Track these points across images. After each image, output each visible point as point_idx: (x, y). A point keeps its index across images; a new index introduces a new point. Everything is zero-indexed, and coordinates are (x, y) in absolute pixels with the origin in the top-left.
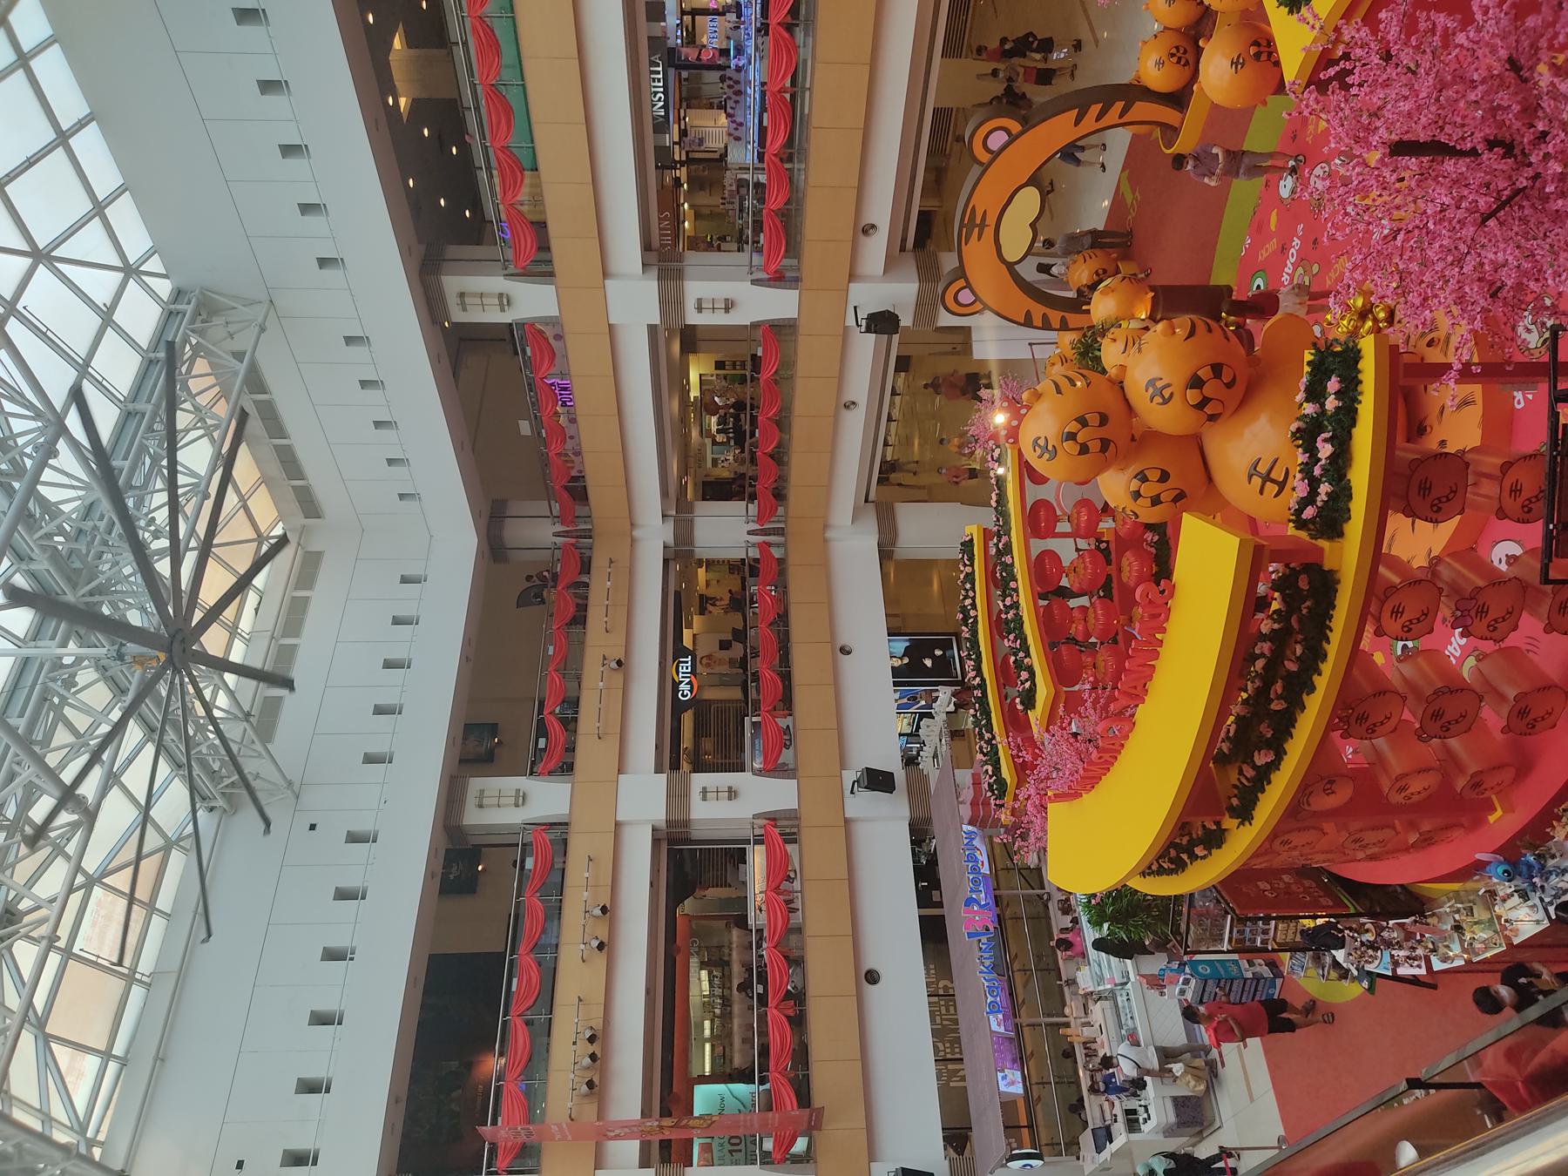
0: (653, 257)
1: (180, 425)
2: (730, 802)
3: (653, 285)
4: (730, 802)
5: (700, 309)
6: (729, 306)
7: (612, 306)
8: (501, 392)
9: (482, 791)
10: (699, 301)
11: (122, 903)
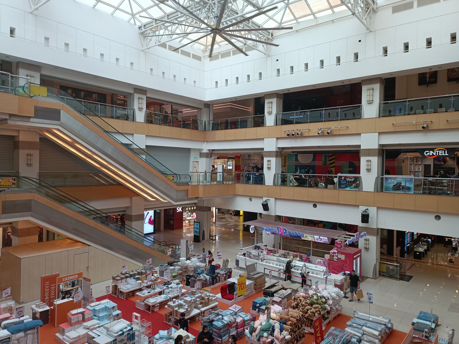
0: (211, 152)
1: (242, 32)
2: (369, 172)
3: (274, 149)
4: (369, 172)
5: (268, 161)
6: (269, 168)
7: (269, 140)
8: (244, 112)
10: (270, 161)
11: (116, 5)
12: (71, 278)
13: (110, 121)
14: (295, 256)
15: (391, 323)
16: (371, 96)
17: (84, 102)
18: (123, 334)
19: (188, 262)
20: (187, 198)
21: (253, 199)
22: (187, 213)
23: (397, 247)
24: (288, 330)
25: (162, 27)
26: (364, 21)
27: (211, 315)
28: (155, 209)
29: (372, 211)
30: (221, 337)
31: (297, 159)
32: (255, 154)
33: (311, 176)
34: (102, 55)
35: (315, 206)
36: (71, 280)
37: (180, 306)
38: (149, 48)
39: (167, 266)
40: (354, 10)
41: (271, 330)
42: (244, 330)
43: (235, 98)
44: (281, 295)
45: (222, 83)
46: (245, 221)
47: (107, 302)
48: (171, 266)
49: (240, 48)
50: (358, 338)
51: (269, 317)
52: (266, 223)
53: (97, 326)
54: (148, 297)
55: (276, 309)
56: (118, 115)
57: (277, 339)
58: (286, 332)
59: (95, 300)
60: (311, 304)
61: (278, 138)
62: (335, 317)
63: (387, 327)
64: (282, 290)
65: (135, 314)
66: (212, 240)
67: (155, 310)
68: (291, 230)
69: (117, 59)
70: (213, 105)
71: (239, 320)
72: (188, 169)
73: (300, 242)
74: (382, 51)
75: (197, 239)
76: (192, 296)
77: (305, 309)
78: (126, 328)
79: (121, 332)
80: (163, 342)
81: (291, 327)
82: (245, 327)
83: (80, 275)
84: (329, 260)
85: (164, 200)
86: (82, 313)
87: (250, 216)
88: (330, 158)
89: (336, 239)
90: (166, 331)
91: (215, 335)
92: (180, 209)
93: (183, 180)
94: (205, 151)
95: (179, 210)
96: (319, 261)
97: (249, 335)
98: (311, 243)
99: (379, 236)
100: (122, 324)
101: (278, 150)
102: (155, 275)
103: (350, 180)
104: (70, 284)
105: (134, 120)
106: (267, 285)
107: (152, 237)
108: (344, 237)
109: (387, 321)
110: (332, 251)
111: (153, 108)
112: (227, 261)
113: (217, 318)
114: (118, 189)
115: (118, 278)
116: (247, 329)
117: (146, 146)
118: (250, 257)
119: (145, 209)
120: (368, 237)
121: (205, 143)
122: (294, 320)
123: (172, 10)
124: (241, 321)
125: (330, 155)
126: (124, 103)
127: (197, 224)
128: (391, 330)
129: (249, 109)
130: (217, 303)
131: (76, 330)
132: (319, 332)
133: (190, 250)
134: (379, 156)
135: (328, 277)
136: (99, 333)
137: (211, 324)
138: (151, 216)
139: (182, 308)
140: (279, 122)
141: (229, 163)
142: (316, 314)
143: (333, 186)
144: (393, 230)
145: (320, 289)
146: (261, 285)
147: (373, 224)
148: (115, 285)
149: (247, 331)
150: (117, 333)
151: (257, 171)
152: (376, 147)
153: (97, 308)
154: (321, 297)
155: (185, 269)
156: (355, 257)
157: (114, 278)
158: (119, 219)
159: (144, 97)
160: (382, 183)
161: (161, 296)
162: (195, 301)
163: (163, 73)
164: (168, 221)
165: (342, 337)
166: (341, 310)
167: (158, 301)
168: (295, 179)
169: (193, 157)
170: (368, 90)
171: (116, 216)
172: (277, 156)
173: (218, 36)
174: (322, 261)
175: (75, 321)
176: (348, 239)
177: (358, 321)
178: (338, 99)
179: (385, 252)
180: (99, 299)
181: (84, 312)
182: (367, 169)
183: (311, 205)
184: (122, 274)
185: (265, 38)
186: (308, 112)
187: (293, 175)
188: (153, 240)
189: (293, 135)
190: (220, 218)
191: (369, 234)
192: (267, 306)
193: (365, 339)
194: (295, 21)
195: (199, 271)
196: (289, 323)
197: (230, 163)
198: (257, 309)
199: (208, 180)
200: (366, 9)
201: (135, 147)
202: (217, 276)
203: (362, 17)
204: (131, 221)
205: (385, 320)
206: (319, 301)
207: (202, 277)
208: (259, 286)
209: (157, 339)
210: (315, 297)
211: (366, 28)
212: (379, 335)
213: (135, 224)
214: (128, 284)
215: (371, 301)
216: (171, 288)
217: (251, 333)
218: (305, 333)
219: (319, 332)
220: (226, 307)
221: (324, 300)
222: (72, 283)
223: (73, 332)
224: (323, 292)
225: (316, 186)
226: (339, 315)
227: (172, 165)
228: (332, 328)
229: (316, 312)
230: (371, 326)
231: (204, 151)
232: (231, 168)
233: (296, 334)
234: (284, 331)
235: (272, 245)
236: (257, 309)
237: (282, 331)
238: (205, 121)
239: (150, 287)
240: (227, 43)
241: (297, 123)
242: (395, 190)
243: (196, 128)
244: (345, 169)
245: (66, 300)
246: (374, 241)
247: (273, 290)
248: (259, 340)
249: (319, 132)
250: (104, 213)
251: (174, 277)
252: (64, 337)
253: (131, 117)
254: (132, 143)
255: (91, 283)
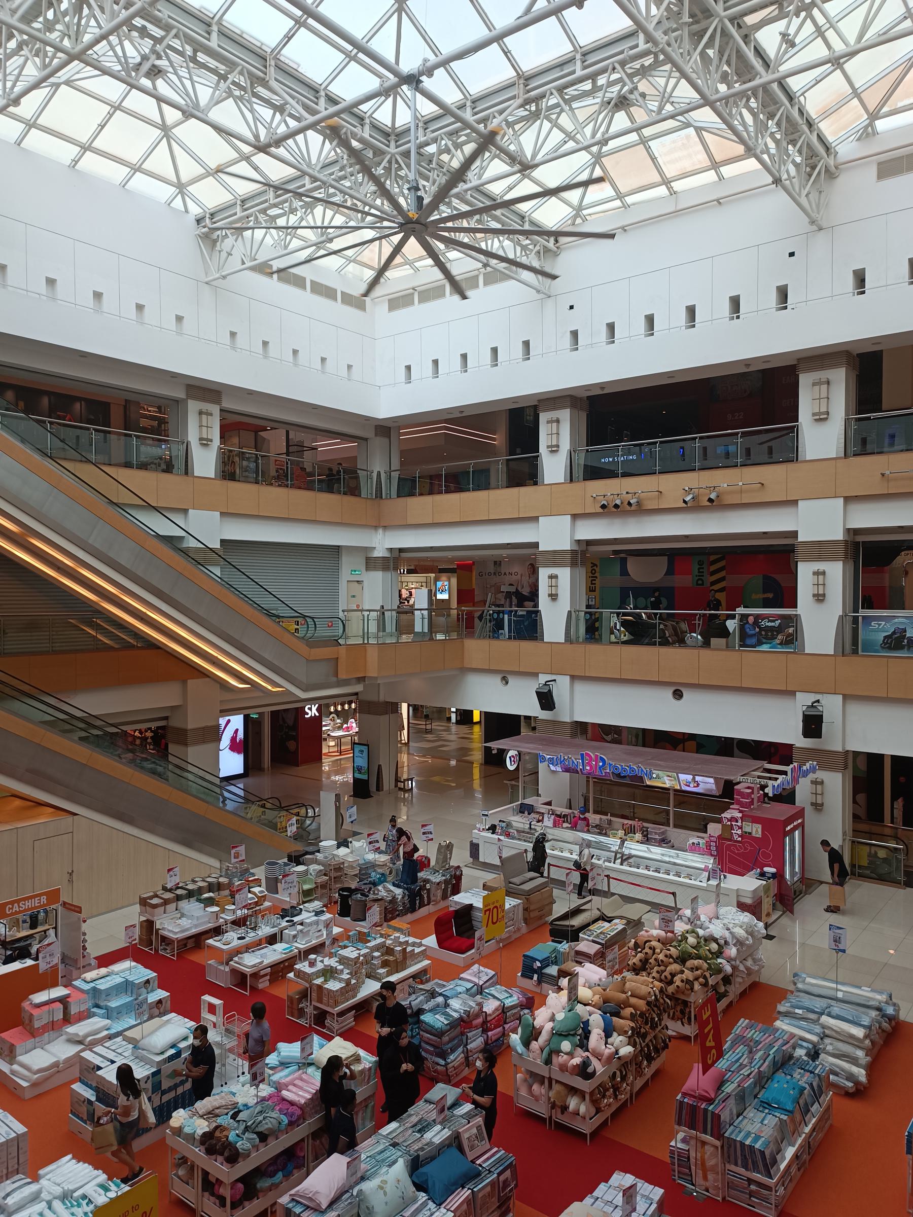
0: (396, 554)
2: (821, 604)
3: (566, 546)
4: (821, 604)
5: (551, 577)
6: (554, 597)
7: (551, 521)
8: (486, 446)
9: (211, 415)
10: (556, 577)
12: (28, 904)
13: (123, 474)
14: (630, 831)
15: (894, 1005)
16: (555, 436)
17: (51, 423)
18: (178, 1055)
19: (343, 851)
20: (335, 679)
21: (511, 680)
22: (333, 720)
23: (894, 799)
24: (626, 1032)
25: (262, 218)
26: (804, 201)
27: (414, 996)
28: (247, 712)
29: (831, 707)
30: (443, 1055)
31: (624, 572)
32: (513, 559)
33: (665, 617)
34: (98, 296)
35: (678, 695)
36: (29, 909)
37: (329, 973)
38: (224, 277)
39: (285, 864)
40: (779, 171)
41: (580, 1033)
42: (504, 1035)
43: (461, 409)
44: (597, 936)
45: (422, 370)
46: (488, 737)
47: (130, 969)
48: (299, 863)
49: (457, 278)
50: (810, 1046)
51: (573, 998)
52: (549, 743)
53: (105, 1033)
54: (238, 951)
55: (590, 974)
56: (143, 459)
57: (598, 1056)
58: (621, 1038)
59: (94, 963)
60: (682, 959)
61: (575, 517)
62: (744, 992)
63: (884, 1016)
64: (600, 923)
65: (207, 998)
66: (404, 790)
67: (261, 986)
68: (617, 760)
69: (140, 308)
70: (400, 428)
71: (490, 1006)
72: (336, 601)
73: (637, 791)
74: (850, 280)
75: (361, 789)
76: (360, 945)
77: (667, 973)
78: (185, 1038)
79: (172, 1051)
80: (290, 1074)
81: (632, 1024)
82: (507, 1026)
83: (53, 896)
84: (719, 837)
85: (273, 686)
86: (63, 1000)
87: (502, 725)
88: (712, 568)
89: (739, 783)
90: (297, 1045)
91: (427, 1051)
92: (314, 709)
93: (323, 632)
94: (380, 553)
95: (312, 711)
96: (696, 841)
97: (520, 1048)
98: (672, 793)
99: (850, 772)
100: (174, 1030)
101: (575, 548)
102: (256, 890)
103: (770, 624)
104: (24, 922)
105: (187, 470)
106: (559, 909)
107: (241, 786)
108: (759, 777)
109: (882, 998)
110: (727, 815)
111: (236, 440)
112: (450, 847)
113: (432, 1003)
114: (148, 659)
115: (155, 901)
116: (514, 1031)
117: (222, 541)
118: (508, 835)
119: (221, 711)
120: (820, 775)
121: (380, 531)
122: (641, 1004)
123: (290, 172)
124: (496, 1009)
125: (713, 558)
126: (159, 425)
127: (363, 748)
128: (893, 1023)
129: (494, 440)
130: (426, 962)
131: (47, 1047)
132: (710, 1037)
133: (347, 820)
134: (845, 559)
135: (722, 885)
136: (111, 1055)
137: (415, 1019)
138: (237, 731)
139: (335, 979)
140: (579, 472)
141: (439, 584)
142: (697, 986)
143: (723, 641)
144: (882, 756)
145: (703, 918)
146: (541, 909)
147: (834, 739)
148: (147, 921)
149: (515, 1039)
150: (162, 1053)
151: (520, 605)
152: (839, 536)
153: (103, 985)
154: (706, 940)
155: (337, 870)
156: (788, 828)
157: (143, 902)
158: (149, 740)
159: (215, 409)
160: (855, 632)
161: (275, 947)
162: (368, 958)
163: (265, 344)
164: (282, 742)
165: (771, 1046)
166: (759, 971)
167: (266, 962)
168: (624, 624)
169: (348, 569)
170: (814, 384)
171: (141, 732)
172: (573, 564)
173: (412, 240)
174: (702, 841)
175: (44, 1022)
176: (770, 783)
177: (807, 1001)
178: (737, 409)
179: (862, 813)
180: (106, 960)
181: (68, 996)
182: (814, 595)
183: (668, 693)
184: (165, 889)
185: (537, 248)
186: (657, 446)
187: (618, 614)
188: (241, 793)
189: (616, 506)
190: (419, 731)
191: (823, 766)
192: (563, 967)
193: (829, 1048)
194: (618, 203)
195: (374, 876)
196: (628, 1011)
197: (443, 583)
198: (535, 977)
199: (388, 629)
200: (808, 169)
201: (193, 544)
202: (423, 888)
203: (797, 189)
204: (186, 745)
205: (879, 997)
206: (701, 951)
207: (381, 891)
208: (536, 914)
209: (272, 1068)
210: (692, 940)
211: (807, 220)
212: (866, 1037)
213: (194, 753)
214: (183, 915)
215: (841, 947)
216: (302, 924)
217: (526, 1044)
218: (670, 1037)
219: (710, 1037)
220: (453, 973)
221: (714, 947)
222: (31, 917)
223: (38, 1051)
224: (711, 926)
225: (680, 641)
226: (755, 986)
227: (292, 591)
228: (743, 1022)
229: (697, 979)
230: (843, 1014)
231: (376, 554)
232: (445, 596)
233: (647, 1040)
234: (615, 1034)
235: (565, 802)
236: (535, 977)
237: (610, 1036)
238: (379, 474)
239: (245, 925)
240: (430, 261)
241: (625, 475)
242: (890, 648)
243: (354, 491)
244: (754, 596)
245: (16, 966)
246: (836, 785)
247: (576, 922)
248: (548, 1062)
249: (687, 499)
250: (112, 725)
251: (308, 896)
252: (15, 1067)
253: (179, 464)
254: (183, 534)
255: (82, 916)
